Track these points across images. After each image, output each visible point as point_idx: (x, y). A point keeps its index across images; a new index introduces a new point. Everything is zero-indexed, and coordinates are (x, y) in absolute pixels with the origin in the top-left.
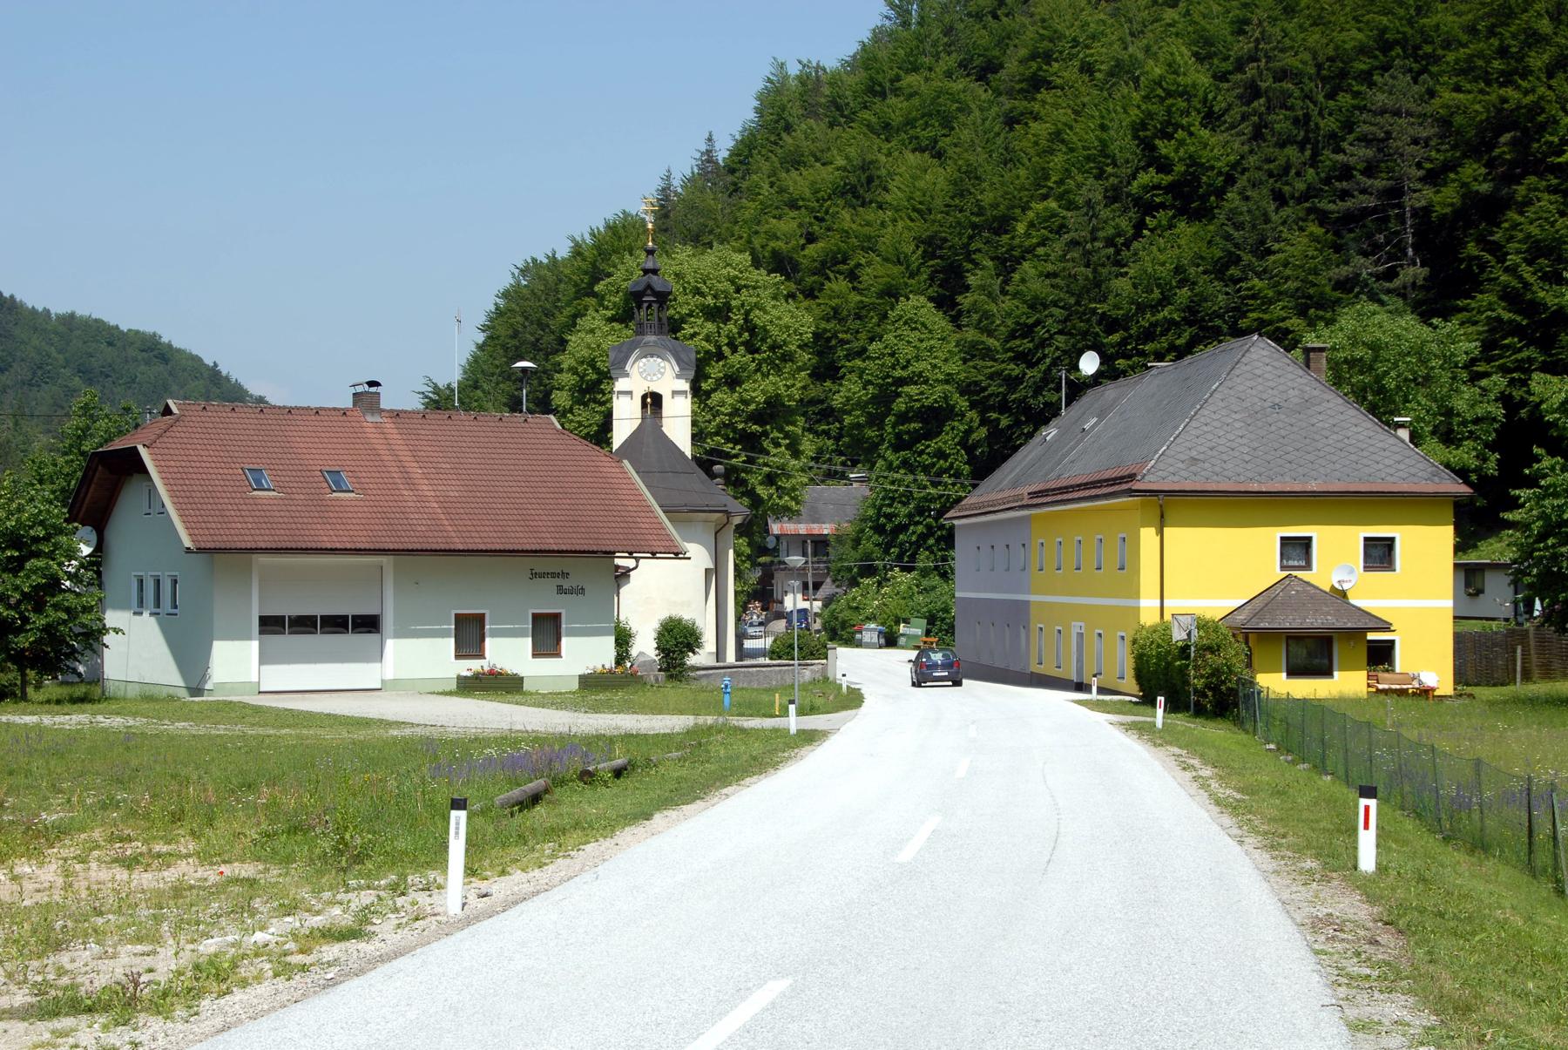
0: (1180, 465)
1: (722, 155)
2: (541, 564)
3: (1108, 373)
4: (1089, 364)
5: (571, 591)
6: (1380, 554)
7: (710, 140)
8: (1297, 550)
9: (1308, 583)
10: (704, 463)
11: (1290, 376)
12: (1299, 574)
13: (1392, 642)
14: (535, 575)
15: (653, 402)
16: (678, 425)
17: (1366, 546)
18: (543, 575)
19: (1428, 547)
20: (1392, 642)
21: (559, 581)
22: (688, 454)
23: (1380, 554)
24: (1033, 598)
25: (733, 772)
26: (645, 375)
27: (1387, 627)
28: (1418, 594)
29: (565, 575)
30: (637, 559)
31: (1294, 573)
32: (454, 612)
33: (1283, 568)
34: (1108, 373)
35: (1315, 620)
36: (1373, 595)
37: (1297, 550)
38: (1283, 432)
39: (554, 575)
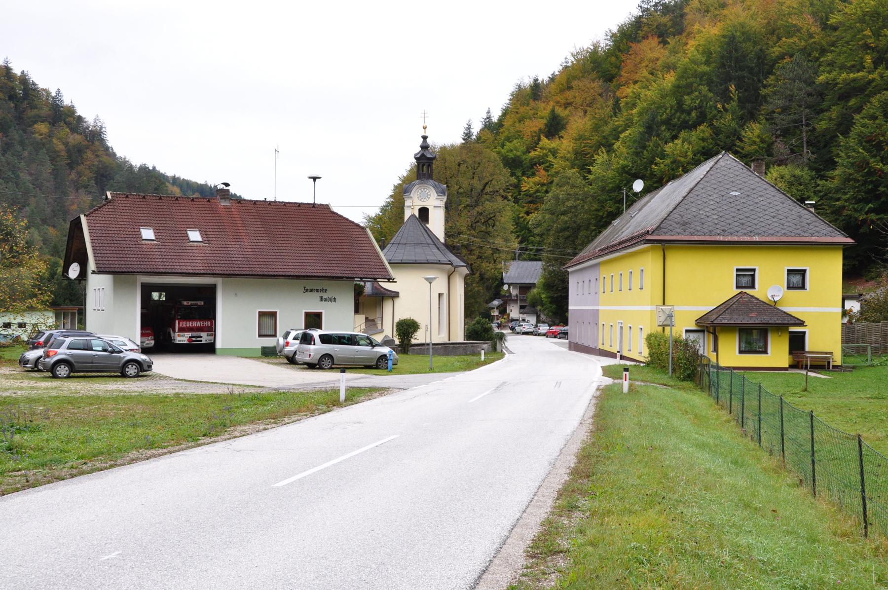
0: (675, 225)
1: (495, 119)
2: (311, 284)
3: (647, 190)
4: (638, 186)
5: (328, 300)
6: (797, 280)
7: (488, 112)
8: (746, 278)
9: (752, 296)
10: (450, 247)
11: (744, 175)
12: (748, 291)
13: (804, 333)
14: (306, 290)
15: (424, 213)
16: (437, 224)
17: (788, 274)
18: (311, 291)
19: (826, 272)
20: (804, 333)
21: (321, 294)
22: (443, 241)
23: (797, 280)
24: (600, 308)
25: (287, 414)
26: (421, 198)
27: (802, 324)
28: (822, 303)
29: (324, 291)
30: (365, 282)
31: (744, 290)
32: (258, 311)
33: (737, 287)
34: (647, 190)
35: (754, 318)
36: (795, 305)
37: (746, 278)
38: (738, 207)
39: (318, 291)
